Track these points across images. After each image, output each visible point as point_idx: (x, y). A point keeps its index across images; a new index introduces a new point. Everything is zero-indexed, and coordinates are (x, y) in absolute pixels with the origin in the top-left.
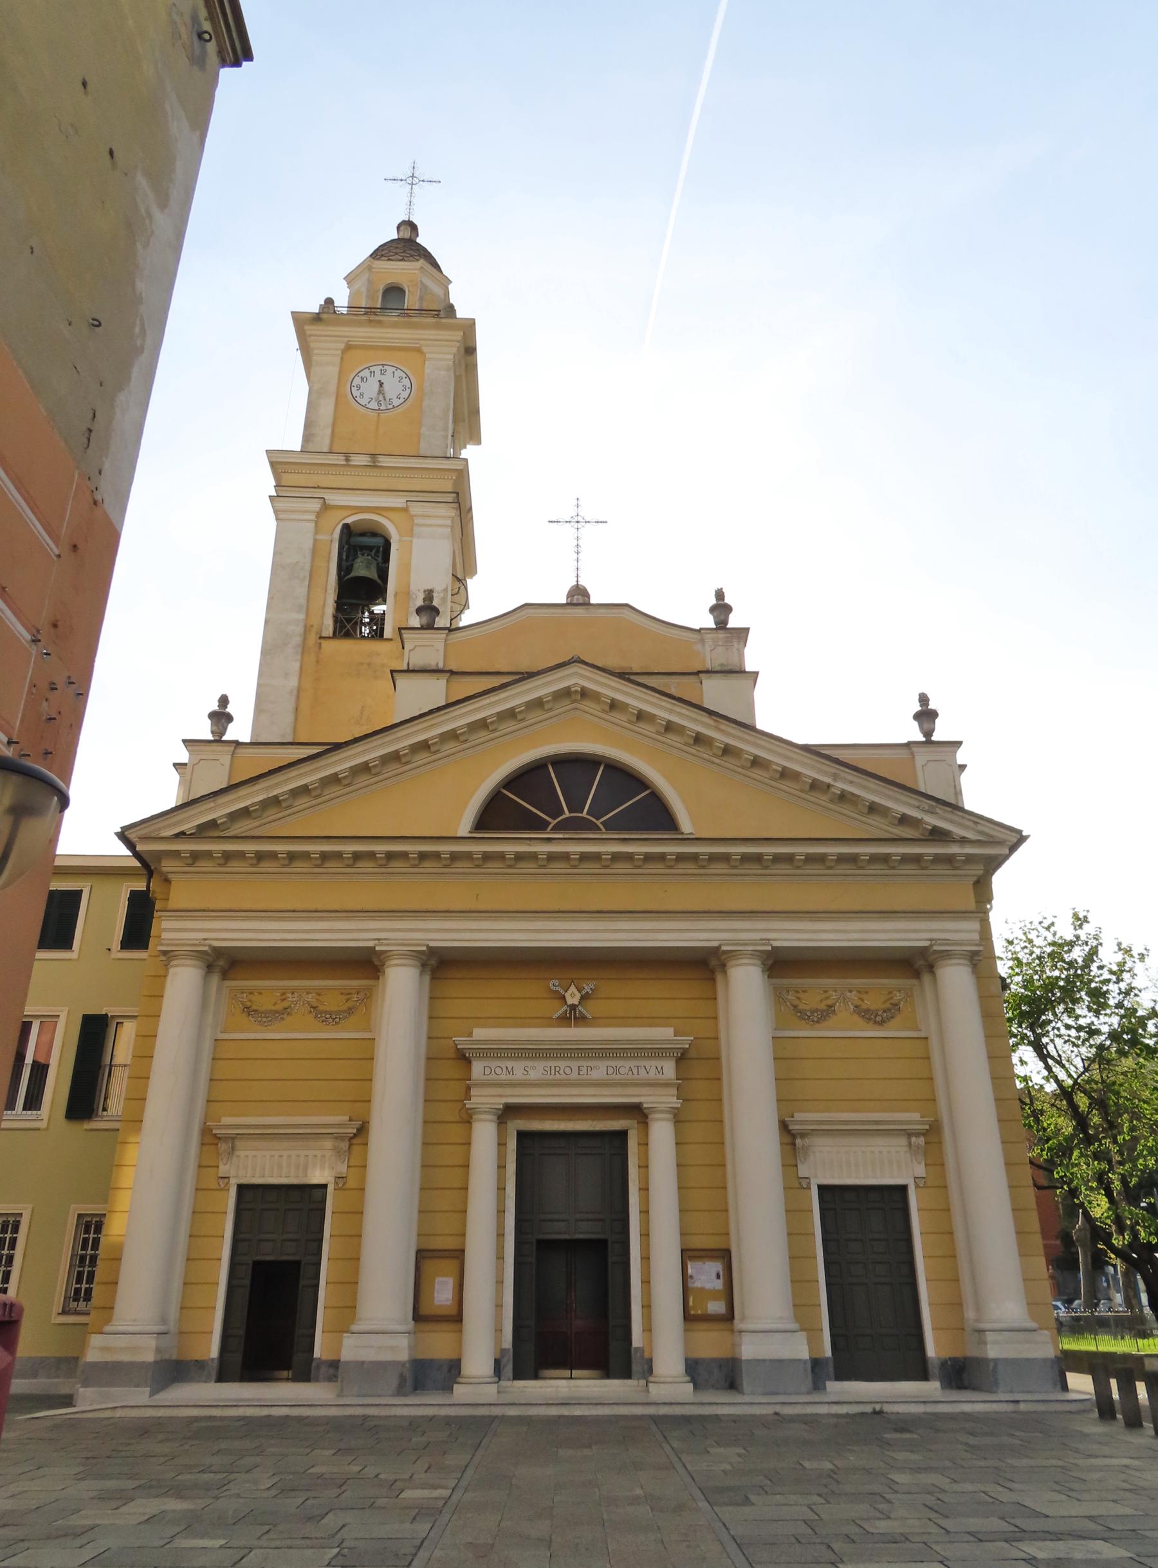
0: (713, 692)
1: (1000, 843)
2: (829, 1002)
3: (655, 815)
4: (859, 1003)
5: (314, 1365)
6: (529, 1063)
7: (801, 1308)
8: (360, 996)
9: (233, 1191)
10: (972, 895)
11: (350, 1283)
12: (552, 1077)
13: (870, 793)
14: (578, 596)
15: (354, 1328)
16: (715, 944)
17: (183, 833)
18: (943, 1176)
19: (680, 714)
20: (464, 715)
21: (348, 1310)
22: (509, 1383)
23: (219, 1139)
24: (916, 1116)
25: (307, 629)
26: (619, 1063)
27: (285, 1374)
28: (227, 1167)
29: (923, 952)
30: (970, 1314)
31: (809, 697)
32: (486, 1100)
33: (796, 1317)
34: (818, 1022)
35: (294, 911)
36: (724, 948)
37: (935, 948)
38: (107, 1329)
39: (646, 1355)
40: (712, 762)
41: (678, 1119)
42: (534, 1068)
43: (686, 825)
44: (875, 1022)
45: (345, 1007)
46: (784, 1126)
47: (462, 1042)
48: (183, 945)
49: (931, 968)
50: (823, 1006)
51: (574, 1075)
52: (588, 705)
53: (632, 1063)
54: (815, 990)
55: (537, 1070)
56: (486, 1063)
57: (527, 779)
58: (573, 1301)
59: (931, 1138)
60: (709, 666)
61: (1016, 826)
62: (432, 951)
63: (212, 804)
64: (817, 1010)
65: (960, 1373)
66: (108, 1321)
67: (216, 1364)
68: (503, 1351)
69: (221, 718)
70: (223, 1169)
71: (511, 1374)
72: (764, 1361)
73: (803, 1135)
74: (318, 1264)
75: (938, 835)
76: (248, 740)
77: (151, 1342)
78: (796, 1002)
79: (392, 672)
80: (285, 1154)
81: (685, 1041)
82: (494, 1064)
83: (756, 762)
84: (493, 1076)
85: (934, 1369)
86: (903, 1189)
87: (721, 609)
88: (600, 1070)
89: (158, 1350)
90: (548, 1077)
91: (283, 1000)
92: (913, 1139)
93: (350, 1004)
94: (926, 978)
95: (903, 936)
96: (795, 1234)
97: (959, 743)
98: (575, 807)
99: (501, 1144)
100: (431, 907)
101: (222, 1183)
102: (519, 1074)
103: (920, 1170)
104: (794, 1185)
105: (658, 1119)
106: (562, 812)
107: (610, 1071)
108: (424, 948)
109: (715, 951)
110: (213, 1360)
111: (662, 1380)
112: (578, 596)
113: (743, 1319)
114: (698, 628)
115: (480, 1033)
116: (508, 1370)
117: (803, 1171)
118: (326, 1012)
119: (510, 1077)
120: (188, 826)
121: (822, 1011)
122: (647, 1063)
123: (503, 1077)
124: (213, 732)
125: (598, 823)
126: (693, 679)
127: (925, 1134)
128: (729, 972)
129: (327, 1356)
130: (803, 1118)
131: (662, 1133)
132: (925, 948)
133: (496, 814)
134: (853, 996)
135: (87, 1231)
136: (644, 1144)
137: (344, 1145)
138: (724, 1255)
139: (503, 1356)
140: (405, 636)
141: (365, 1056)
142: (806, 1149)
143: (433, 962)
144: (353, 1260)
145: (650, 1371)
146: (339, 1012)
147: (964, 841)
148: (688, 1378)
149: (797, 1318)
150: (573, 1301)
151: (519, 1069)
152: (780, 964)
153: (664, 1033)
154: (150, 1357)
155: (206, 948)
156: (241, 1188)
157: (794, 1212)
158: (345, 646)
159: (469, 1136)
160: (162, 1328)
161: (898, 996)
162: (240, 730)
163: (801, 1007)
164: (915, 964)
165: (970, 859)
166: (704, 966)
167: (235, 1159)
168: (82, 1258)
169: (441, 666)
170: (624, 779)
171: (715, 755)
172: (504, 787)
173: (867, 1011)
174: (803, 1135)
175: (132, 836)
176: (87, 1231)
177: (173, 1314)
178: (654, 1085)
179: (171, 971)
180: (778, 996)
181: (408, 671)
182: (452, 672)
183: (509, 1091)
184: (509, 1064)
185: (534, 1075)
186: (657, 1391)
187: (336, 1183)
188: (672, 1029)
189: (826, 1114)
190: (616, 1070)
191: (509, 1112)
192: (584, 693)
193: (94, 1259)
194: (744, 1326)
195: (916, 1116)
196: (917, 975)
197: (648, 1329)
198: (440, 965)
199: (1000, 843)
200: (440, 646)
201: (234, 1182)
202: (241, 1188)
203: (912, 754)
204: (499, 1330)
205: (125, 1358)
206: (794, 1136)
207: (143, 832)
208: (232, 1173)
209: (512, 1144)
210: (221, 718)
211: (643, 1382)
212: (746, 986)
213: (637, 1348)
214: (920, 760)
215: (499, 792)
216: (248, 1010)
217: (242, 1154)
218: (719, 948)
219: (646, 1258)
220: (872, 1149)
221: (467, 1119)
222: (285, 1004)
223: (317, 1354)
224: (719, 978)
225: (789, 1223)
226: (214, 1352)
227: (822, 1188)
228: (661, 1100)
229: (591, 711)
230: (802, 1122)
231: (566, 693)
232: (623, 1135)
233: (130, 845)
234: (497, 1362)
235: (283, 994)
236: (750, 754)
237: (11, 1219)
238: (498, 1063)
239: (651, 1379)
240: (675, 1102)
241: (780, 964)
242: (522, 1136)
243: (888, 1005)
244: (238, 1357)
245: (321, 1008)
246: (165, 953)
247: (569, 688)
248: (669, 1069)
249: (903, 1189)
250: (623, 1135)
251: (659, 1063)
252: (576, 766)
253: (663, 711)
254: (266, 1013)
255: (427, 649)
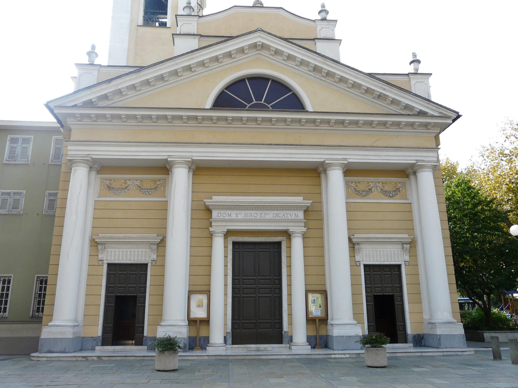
0: (321, 47)
1: (449, 117)
2: (370, 188)
3: (295, 103)
4: (382, 188)
5: (144, 339)
6: (238, 212)
7: (356, 315)
8: (161, 182)
9: (105, 267)
10: (434, 142)
11: (160, 305)
12: (248, 218)
13: (392, 94)
14: (258, 5)
15: (162, 324)
16: (322, 160)
17: (76, 105)
18: (416, 260)
19: (308, 56)
20: (207, 53)
21: (159, 317)
22: (230, 346)
23: (98, 244)
24: (406, 236)
25: (132, 21)
26: (278, 212)
27: (131, 342)
28: (102, 256)
29: (413, 165)
30: (426, 317)
31: (367, 47)
32: (218, 229)
33: (354, 318)
34: (365, 196)
35: (129, 142)
36: (327, 162)
37: (419, 163)
38: (50, 324)
39: (290, 335)
40: (321, 80)
41: (304, 237)
42: (240, 214)
43: (309, 107)
44: (389, 196)
45: (153, 187)
46: (350, 240)
47: (208, 202)
48: (78, 157)
49: (415, 173)
50: (367, 189)
51: (259, 217)
52: (264, 52)
53: (285, 212)
54: (364, 181)
55: (241, 215)
56: (219, 211)
57: (237, 85)
58: (257, 313)
59: (161, 244)
60: (318, 37)
61: (456, 110)
62: (193, 162)
63: (90, 92)
64: (364, 191)
65: (420, 341)
66: (51, 320)
67: (101, 338)
68: (227, 333)
69: (92, 53)
70: (100, 257)
71: (231, 342)
72: (343, 336)
73: (358, 244)
74: (145, 297)
75: (422, 114)
76: (106, 65)
77: (71, 330)
78: (356, 187)
79: (173, 34)
80: (128, 250)
81: (308, 203)
82: (222, 212)
83: (342, 80)
84: (222, 217)
85: (410, 338)
86: (399, 266)
87: (323, 11)
88: (270, 215)
89: (74, 333)
90: (247, 218)
91: (125, 183)
92: (405, 245)
93: (156, 186)
94: (412, 177)
95: (405, 158)
96: (354, 285)
97: (431, 74)
98: (259, 98)
99: (226, 247)
100: (193, 141)
101: (100, 263)
102: (234, 216)
103: (407, 258)
104: (354, 264)
105: (296, 236)
106: (252, 101)
107: (275, 215)
108: (190, 160)
109: (322, 164)
110: (99, 337)
111: (295, 344)
112: (258, 5)
113: (332, 319)
114: (314, 19)
115: (217, 199)
116: (230, 340)
117: (357, 258)
118: (146, 189)
119: (229, 218)
120: (79, 102)
121: (367, 191)
122: (291, 212)
123: (226, 218)
124: (89, 61)
125: (269, 106)
126: (312, 42)
127: (410, 243)
128: (327, 173)
129: (150, 335)
130: (358, 236)
131: (297, 243)
132: (414, 164)
133: (222, 101)
134: (380, 185)
135: (41, 283)
136: (289, 247)
137: (155, 247)
138: (324, 293)
139: (227, 335)
140: (178, 19)
141: (163, 209)
142: (359, 250)
143: (193, 167)
144: (160, 295)
145: (291, 340)
146: (151, 189)
147: (433, 116)
148: (308, 344)
149: (355, 319)
150: (257, 313)
151: (234, 215)
152: (350, 171)
153: (299, 199)
154: (70, 336)
155: (89, 158)
156: (109, 265)
157: (354, 276)
158: (149, 30)
159: (211, 243)
160: (76, 324)
161: (399, 185)
162: (102, 60)
163: (358, 189)
164: (406, 172)
165: (436, 125)
166: (315, 172)
167: (106, 253)
168: (40, 295)
169: (196, 33)
170: (280, 87)
171: (323, 76)
172: (225, 89)
173: (386, 191)
174: (358, 244)
175: (52, 106)
176: (41, 283)
177: (80, 318)
178: (293, 221)
179: (73, 169)
180: (347, 184)
181: (180, 34)
182: (201, 36)
183: (229, 224)
184: (229, 212)
185: (240, 217)
186: (295, 350)
187: (152, 263)
188: (302, 198)
189: (396, 235)
190: (277, 215)
191: (228, 233)
192: (264, 47)
193: (45, 295)
194: (332, 322)
195: (406, 236)
196: (408, 176)
197: (290, 324)
198: (199, 169)
199: (449, 117)
200: (195, 24)
201: (105, 262)
202: (109, 265)
203: (410, 79)
204: (225, 325)
205: (59, 336)
206: (354, 244)
207: (57, 104)
208: (105, 259)
209: (230, 247)
210: (92, 53)
211: (288, 345)
212: (336, 179)
213: (285, 332)
214: (413, 82)
215: (223, 91)
216: (109, 188)
217: (109, 250)
218: (324, 162)
219: (290, 295)
220: (387, 249)
221: (211, 236)
222: (126, 185)
223: (145, 334)
224: (323, 176)
225: (352, 280)
226: (100, 333)
227: (365, 266)
228: (297, 229)
229: (266, 54)
230: (358, 238)
231: (254, 46)
232: (279, 244)
233: (52, 111)
234: (225, 338)
235: (125, 181)
236: (339, 75)
237: (7, 279)
238: (224, 212)
239: (291, 344)
240: (304, 229)
241: (350, 171)
242: (234, 243)
243: (395, 189)
244: (110, 335)
245: (143, 187)
246: (70, 161)
247: (256, 43)
248: (301, 215)
249: (399, 266)
250: (279, 244)
251: (296, 212)
252: (258, 81)
253: (300, 54)
254: (118, 189)
255: (190, 26)
